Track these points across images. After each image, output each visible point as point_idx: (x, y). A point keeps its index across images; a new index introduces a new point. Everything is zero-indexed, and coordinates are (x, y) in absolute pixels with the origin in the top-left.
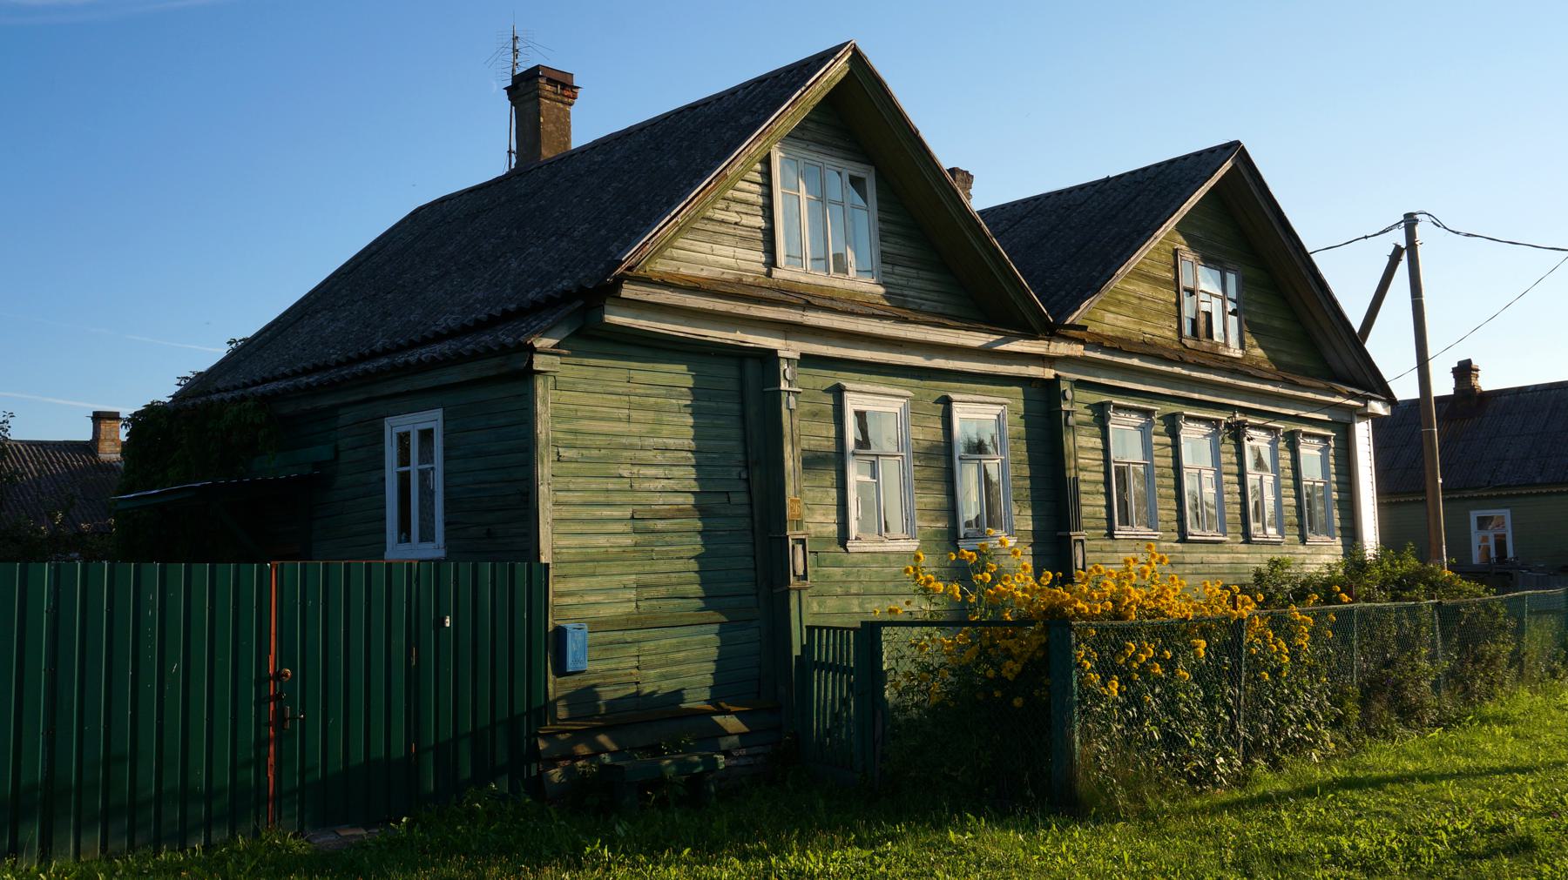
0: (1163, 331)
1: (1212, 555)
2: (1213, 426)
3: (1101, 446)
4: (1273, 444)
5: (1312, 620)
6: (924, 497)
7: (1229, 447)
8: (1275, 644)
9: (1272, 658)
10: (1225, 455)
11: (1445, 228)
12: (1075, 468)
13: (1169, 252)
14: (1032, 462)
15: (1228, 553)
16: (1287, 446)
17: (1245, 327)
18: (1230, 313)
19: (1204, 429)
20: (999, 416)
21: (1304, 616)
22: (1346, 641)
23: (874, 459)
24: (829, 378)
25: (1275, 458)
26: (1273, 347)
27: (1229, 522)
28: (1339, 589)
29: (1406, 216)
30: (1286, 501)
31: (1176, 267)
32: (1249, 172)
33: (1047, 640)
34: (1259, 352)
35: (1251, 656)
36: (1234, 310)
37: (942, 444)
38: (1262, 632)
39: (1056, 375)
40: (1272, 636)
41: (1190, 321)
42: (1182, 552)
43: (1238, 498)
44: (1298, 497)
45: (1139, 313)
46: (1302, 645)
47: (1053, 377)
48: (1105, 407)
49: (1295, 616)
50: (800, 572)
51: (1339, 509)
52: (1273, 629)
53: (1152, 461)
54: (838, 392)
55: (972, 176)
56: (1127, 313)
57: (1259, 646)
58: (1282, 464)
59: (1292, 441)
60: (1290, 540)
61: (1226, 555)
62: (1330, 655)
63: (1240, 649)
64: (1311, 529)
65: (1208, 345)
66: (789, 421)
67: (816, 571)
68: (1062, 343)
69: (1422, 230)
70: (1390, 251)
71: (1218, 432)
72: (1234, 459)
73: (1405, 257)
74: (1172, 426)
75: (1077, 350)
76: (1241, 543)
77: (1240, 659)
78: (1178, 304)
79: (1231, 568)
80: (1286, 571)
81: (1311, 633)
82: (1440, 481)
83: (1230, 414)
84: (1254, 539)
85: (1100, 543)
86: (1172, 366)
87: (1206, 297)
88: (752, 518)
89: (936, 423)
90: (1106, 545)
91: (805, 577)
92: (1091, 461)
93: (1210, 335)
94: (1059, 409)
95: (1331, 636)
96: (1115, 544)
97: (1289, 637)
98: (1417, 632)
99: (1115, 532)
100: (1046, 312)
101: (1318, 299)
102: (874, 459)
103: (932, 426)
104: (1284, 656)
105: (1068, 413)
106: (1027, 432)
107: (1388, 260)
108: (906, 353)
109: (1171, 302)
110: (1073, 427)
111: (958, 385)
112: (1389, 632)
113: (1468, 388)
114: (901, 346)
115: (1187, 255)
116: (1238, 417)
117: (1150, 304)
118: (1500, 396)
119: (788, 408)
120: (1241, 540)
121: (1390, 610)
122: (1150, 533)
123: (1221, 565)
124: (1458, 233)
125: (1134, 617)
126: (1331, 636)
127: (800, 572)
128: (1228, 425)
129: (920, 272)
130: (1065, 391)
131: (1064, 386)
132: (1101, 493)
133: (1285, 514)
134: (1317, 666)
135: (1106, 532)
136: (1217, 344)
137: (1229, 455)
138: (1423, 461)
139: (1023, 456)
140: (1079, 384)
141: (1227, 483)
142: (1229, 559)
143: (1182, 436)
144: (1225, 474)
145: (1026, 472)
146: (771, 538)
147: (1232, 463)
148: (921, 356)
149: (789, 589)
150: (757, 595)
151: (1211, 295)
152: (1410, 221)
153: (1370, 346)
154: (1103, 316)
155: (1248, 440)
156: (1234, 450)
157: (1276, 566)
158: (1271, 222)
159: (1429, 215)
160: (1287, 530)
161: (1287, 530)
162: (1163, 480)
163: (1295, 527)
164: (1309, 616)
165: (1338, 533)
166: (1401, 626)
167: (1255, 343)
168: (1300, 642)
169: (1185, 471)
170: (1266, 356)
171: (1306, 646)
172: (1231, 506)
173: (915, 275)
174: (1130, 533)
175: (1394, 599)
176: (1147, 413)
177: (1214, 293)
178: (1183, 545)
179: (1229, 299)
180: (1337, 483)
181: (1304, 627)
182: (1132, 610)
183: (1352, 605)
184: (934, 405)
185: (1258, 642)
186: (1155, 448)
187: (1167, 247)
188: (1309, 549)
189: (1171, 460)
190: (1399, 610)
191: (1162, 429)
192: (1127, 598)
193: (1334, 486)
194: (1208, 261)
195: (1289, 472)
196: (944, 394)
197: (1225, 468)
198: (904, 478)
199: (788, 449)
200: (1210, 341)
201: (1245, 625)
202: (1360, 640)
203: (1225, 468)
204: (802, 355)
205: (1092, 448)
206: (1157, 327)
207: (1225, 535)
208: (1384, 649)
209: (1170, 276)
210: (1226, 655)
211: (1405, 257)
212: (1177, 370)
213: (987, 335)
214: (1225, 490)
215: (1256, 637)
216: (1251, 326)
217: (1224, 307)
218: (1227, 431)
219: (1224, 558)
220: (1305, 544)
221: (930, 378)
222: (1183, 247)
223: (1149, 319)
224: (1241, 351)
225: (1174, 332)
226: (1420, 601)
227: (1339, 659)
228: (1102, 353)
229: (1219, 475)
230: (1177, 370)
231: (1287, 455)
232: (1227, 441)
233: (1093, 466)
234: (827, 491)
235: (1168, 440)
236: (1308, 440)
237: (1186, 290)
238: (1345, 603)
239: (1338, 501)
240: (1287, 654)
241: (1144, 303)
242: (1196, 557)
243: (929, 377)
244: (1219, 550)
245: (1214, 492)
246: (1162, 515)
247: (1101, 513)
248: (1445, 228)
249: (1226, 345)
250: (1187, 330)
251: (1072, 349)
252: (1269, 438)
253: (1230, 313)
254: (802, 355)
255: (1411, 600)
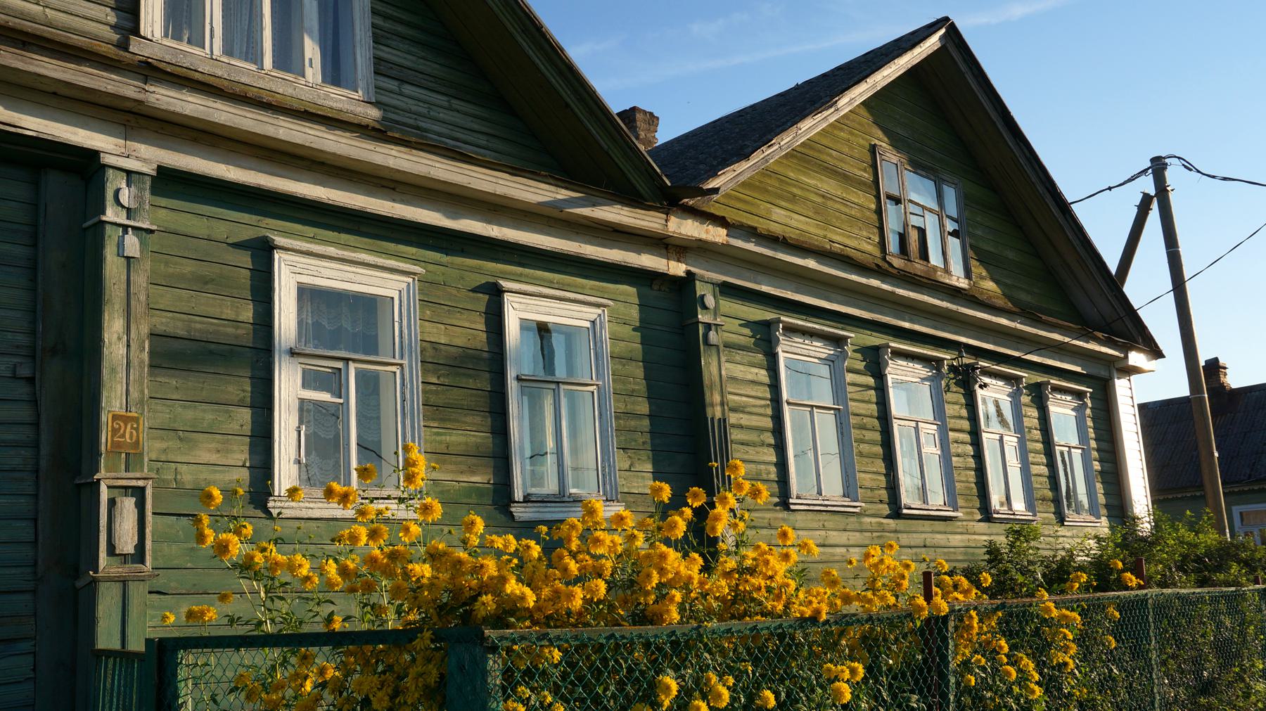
0: (863, 244)
1: (938, 536)
2: (932, 368)
3: (767, 380)
4: (1015, 396)
5: (1079, 618)
6: (445, 434)
7: (955, 397)
8: (1012, 665)
9: (1010, 691)
10: (951, 406)
11: (1198, 172)
12: (722, 404)
13: (863, 147)
14: (653, 396)
15: (962, 533)
16: (1032, 401)
17: (971, 253)
18: (950, 234)
19: (920, 370)
20: (593, 322)
21: (1064, 611)
22: (1138, 653)
23: (340, 365)
24: (247, 225)
25: (1018, 415)
26: (1008, 281)
27: (961, 492)
28: (1120, 565)
29: (1153, 160)
30: (1035, 469)
31: (874, 167)
32: (963, 57)
33: (442, 676)
34: (989, 285)
35: (968, 690)
36: (955, 230)
37: (485, 355)
38: (988, 643)
39: (688, 273)
40: (1006, 649)
41: (897, 237)
42: (896, 531)
43: (971, 462)
44: (1051, 465)
45: (821, 213)
46: (1066, 664)
47: (683, 275)
48: (772, 328)
49: (1048, 610)
50: (127, 543)
51: (1102, 483)
52: (1008, 634)
53: (847, 406)
54: (263, 252)
55: (658, 118)
56: (805, 213)
57: (983, 669)
58: (1027, 422)
59: (1039, 397)
60: (1044, 518)
61: (958, 537)
62: (1114, 680)
63: (943, 677)
64: (1069, 506)
65: (922, 268)
66: (124, 277)
67: (193, 549)
68: (690, 221)
69: (1174, 175)
70: (1138, 199)
71: (939, 375)
72: (964, 413)
73: (1155, 206)
74: (875, 363)
75: (717, 235)
76: (980, 521)
77: (944, 696)
78: (879, 212)
79: (966, 554)
80: (1033, 543)
81: (1081, 640)
82: (1216, 454)
83: (954, 354)
84: (995, 516)
85: (768, 515)
86: (868, 278)
87: (918, 210)
88: (36, 445)
89: (475, 322)
90: (776, 519)
91: (140, 554)
92: (751, 400)
93: (924, 255)
94: (694, 320)
95: (1114, 645)
96: (792, 517)
97: (1040, 651)
98: (1243, 634)
99: (791, 501)
100: (658, 170)
101: (1060, 224)
102: (340, 365)
103: (467, 325)
104: (1032, 686)
105: (708, 327)
106: (645, 352)
107: (1136, 210)
108: (402, 202)
109: (869, 209)
110: (717, 346)
111: (519, 270)
112: (1203, 636)
113: (1217, 385)
114: (394, 189)
115: (888, 155)
116: (967, 360)
117: (837, 206)
118: (1251, 392)
119: (120, 253)
120: (979, 517)
121: (1201, 599)
122: (846, 504)
123: (952, 550)
124: (1214, 177)
125: (675, 616)
126: (1114, 645)
127: (127, 543)
128: (952, 369)
129: (454, 101)
130: (702, 297)
131: (700, 289)
132: (769, 445)
133: (1035, 485)
134: (1094, 700)
135: (777, 500)
136: (935, 269)
137: (957, 407)
138: (1195, 431)
139: (638, 384)
140: (727, 290)
141: (956, 442)
142: (962, 541)
143: (889, 377)
144: (952, 430)
145: (643, 407)
146: (79, 486)
147: (961, 418)
148: (438, 211)
149: (95, 581)
150: (34, 592)
151: (923, 207)
152: (1158, 167)
153: (1129, 289)
154: (769, 211)
155: (981, 387)
156: (963, 401)
157: (1018, 539)
158: (994, 123)
159: (1179, 158)
160: (1039, 506)
161: (1039, 506)
162: (864, 432)
163: (1049, 503)
164: (1073, 610)
165: (1104, 511)
166: (1220, 625)
167: (984, 273)
168: (1061, 657)
169: (896, 423)
170: (999, 291)
171: (1072, 665)
172: (963, 473)
173: (446, 104)
174: (815, 502)
175: (1202, 583)
176: (838, 341)
177: (928, 206)
178: (897, 521)
179: (948, 216)
180: (1098, 450)
181: (1066, 631)
182: (672, 599)
183: (1144, 592)
184: (471, 294)
185: (979, 661)
186: (850, 389)
187: (862, 142)
188: (1068, 531)
189: (874, 407)
190: (1215, 600)
191: (861, 365)
192: (655, 575)
193: (1095, 454)
194: (918, 167)
195: (1037, 434)
196: (492, 280)
197: (952, 423)
198: (403, 400)
199: (113, 327)
200: (925, 263)
201: (951, 629)
202: (1162, 650)
203: (952, 423)
204: (161, 169)
205: (753, 382)
206: (850, 236)
207: (956, 510)
208: (1198, 663)
209: (867, 176)
210: (912, 692)
211: (1155, 206)
212: (875, 283)
213: (553, 188)
214: (953, 450)
215: (976, 652)
216: (976, 253)
217: (942, 226)
218: (952, 376)
219: (956, 540)
220: (1063, 525)
221: (463, 253)
222: (884, 145)
223: (837, 225)
224: (967, 281)
225: (875, 246)
226: (1242, 585)
227: (1131, 684)
228: (757, 244)
229: (943, 430)
230: (875, 283)
231: (1034, 413)
232: (954, 388)
233: (754, 406)
234: (227, 411)
235: (870, 381)
236: (1059, 396)
237: (890, 197)
238: (1132, 589)
239: (1101, 473)
240: (1037, 683)
241: (830, 203)
242: (917, 539)
243: (462, 251)
244: (949, 529)
245: (939, 452)
246: (864, 479)
247: (769, 473)
248: (1198, 172)
249: (947, 271)
250: (893, 245)
251: (707, 232)
252: (1008, 389)
253: (950, 234)
254: (160, 168)
255: (1228, 584)
